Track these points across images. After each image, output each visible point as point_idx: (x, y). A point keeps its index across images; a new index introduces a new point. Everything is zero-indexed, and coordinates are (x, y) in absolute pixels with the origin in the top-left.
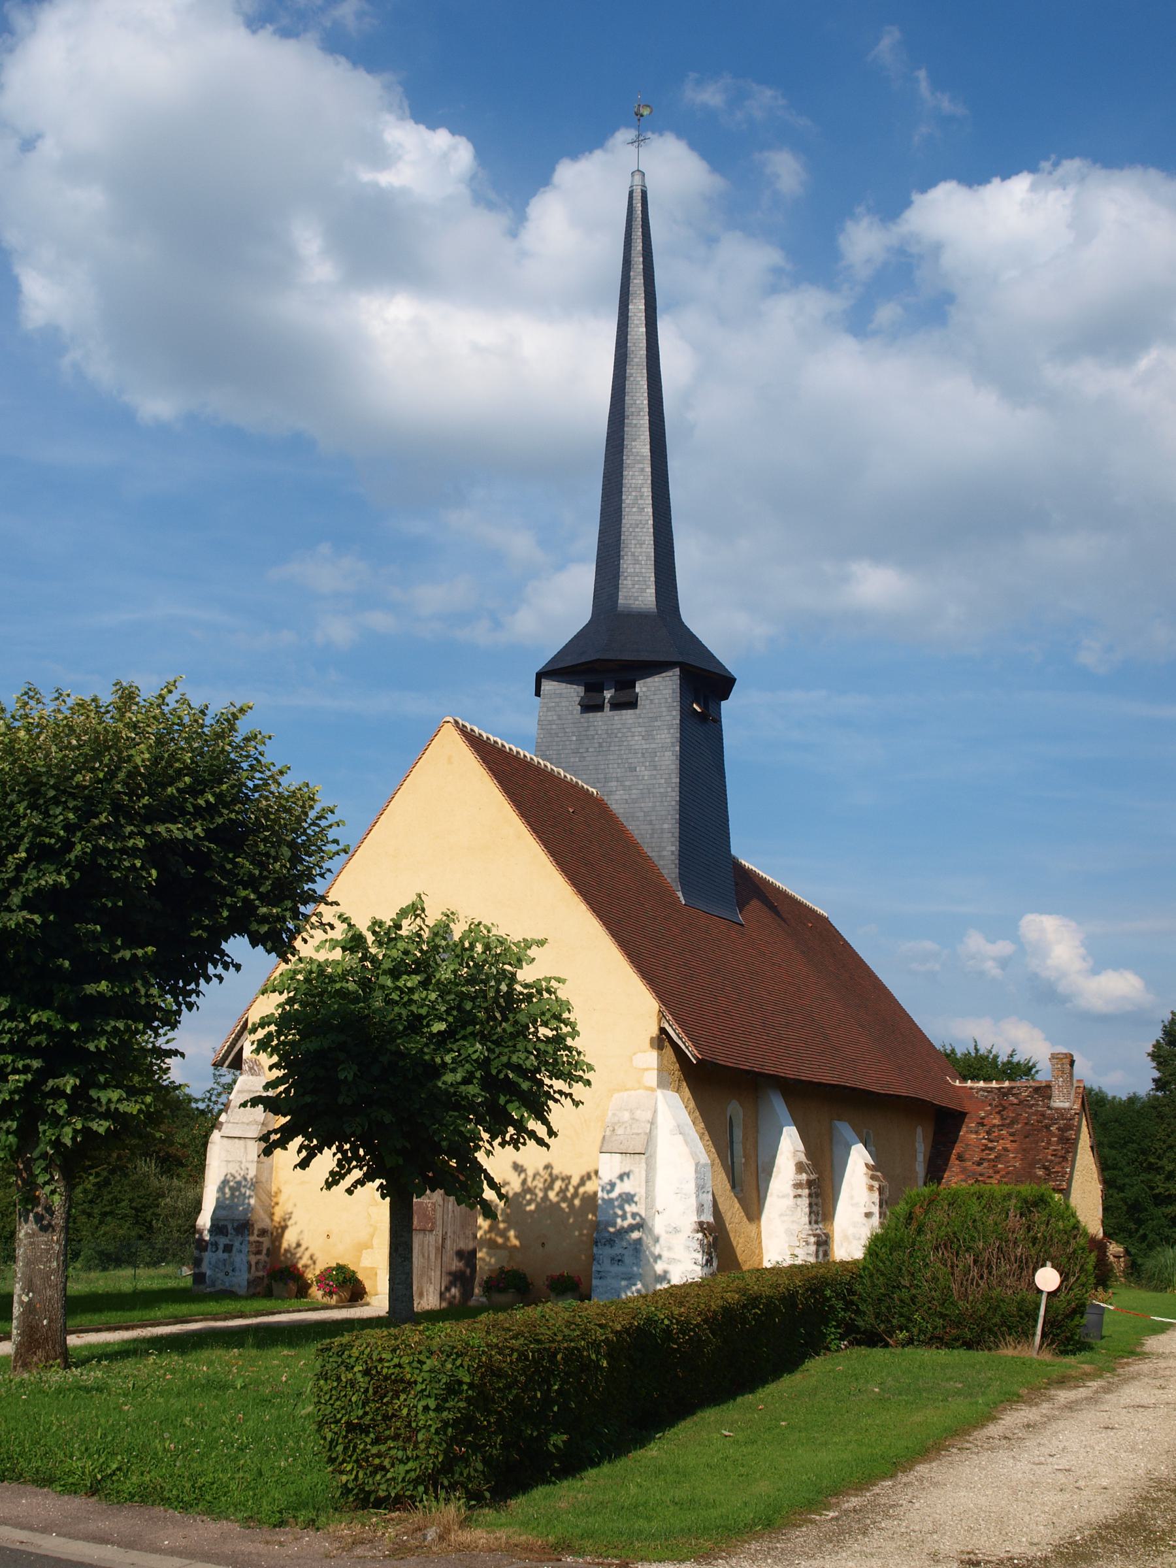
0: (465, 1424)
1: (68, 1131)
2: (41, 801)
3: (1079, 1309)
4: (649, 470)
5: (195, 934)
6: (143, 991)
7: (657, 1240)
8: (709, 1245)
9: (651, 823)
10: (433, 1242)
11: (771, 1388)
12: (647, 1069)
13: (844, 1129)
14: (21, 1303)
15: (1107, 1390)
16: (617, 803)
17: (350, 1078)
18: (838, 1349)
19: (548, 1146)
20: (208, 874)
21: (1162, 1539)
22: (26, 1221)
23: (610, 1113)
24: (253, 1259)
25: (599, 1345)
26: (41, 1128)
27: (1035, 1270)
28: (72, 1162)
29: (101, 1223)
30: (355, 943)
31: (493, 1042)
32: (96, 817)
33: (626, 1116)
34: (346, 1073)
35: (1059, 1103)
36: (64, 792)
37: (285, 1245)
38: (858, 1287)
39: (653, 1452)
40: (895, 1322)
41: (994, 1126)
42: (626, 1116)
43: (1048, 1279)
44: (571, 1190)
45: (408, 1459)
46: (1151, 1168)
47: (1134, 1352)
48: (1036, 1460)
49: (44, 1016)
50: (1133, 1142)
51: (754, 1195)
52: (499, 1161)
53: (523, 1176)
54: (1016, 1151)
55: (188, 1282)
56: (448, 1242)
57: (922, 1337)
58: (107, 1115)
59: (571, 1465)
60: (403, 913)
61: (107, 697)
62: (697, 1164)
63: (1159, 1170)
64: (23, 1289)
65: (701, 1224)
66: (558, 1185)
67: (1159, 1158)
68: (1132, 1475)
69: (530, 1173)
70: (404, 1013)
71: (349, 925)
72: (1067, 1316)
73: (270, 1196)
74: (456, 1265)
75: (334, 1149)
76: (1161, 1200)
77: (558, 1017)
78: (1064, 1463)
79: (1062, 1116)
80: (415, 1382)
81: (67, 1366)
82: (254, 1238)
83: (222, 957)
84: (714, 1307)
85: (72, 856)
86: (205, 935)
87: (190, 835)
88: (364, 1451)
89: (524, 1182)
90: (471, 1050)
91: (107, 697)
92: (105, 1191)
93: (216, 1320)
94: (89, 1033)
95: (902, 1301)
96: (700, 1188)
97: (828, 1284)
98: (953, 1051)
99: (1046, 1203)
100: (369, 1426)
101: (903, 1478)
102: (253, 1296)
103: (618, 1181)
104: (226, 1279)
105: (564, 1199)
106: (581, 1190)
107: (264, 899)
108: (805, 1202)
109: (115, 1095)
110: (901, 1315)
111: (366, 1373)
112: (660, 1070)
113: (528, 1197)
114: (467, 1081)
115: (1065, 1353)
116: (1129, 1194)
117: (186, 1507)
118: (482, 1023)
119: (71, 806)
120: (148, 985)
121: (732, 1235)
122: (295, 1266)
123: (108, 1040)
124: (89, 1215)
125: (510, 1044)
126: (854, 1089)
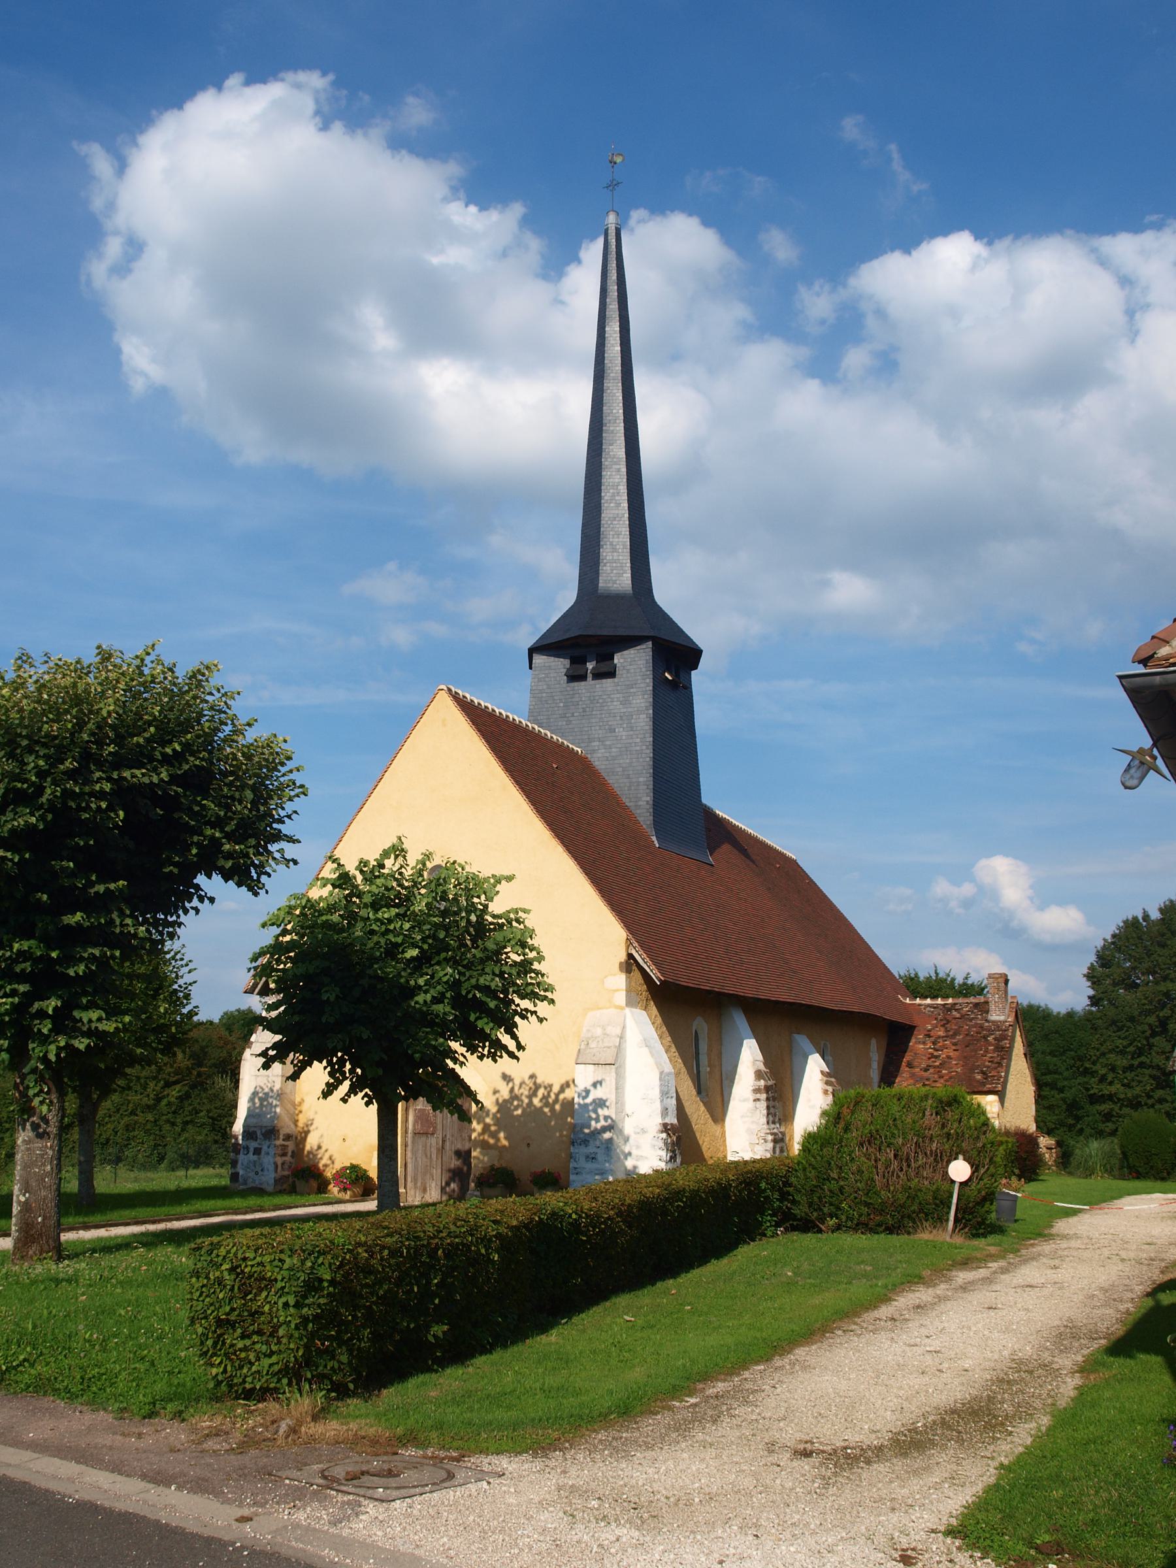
0: (326, 1319)
1: (53, 1047)
2: (18, 751)
3: (990, 1197)
4: (624, 470)
5: (167, 870)
6: (118, 922)
7: (627, 1140)
8: (673, 1143)
9: (628, 777)
10: (434, 1144)
11: (695, 1273)
12: (617, 990)
13: (802, 1041)
14: (19, 1202)
15: (1004, 1271)
16: (599, 760)
17: (332, 999)
18: (775, 1235)
19: (518, 1059)
20: (176, 816)
21: (1002, 1424)
22: (24, 1130)
23: (584, 1030)
24: (279, 1160)
25: (490, 1240)
26: (31, 1046)
27: (949, 1162)
28: (59, 1074)
29: (183, 1130)
30: (344, 879)
31: (464, 966)
32: (62, 763)
33: (599, 1031)
34: (329, 994)
35: (995, 1016)
36: (37, 742)
37: (308, 1148)
38: (793, 1180)
39: (552, 1338)
40: (826, 1210)
41: (939, 1037)
42: (599, 1031)
43: (959, 1170)
44: (553, 1096)
45: (272, 1353)
46: (1086, 1072)
47: (1042, 1233)
48: (912, 1341)
49: (26, 945)
50: (1071, 1050)
51: (719, 1099)
52: (480, 1075)
53: (511, 1085)
54: (958, 1059)
55: (225, 1181)
56: (448, 1144)
57: (849, 1224)
58: (89, 1034)
59: (457, 1352)
60: (386, 854)
61: (90, 658)
62: (661, 1073)
63: (1093, 1074)
64: (20, 1190)
65: (665, 1125)
66: (541, 1092)
67: (1094, 1063)
68: (996, 1357)
69: (517, 1082)
70: (383, 941)
71: (339, 864)
72: (978, 1204)
73: (294, 1105)
74: (455, 1163)
75: (325, 1062)
76: (1094, 1099)
77: (523, 945)
78: (935, 1344)
79: (998, 1028)
80: (276, 1280)
81: (60, 1258)
82: (279, 1142)
83: (197, 891)
84: (628, 1201)
85: (44, 800)
86: (176, 871)
87: (155, 779)
88: (232, 1346)
89: (512, 1090)
90: (441, 974)
91: (90, 658)
92: (186, 1103)
93: (236, 1214)
94: (69, 959)
95: (831, 1191)
96: (664, 1094)
97: (763, 1178)
98: (916, 975)
99: (959, 1103)
100: (235, 1322)
101: (778, 1362)
102: (281, 1192)
103: (592, 1089)
104: (256, 1177)
105: (547, 1104)
106: (561, 1097)
107: (229, 837)
108: (764, 1104)
109: (94, 1015)
110: (831, 1204)
111: (232, 1270)
112: (629, 991)
113: (515, 1103)
114: (437, 1000)
115: (976, 1236)
116: (1068, 1094)
117: (72, 1397)
118: (454, 951)
119: (41, 753)
120: (122, 915)
121: (698, 1135)
122: (316, 1166)
123: (86, 966)
124: (173, 1124)
125: (480, 968)
126: (777, 1002)
